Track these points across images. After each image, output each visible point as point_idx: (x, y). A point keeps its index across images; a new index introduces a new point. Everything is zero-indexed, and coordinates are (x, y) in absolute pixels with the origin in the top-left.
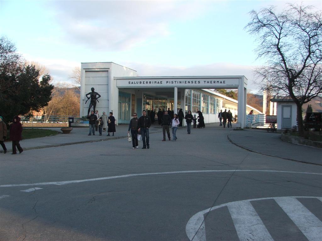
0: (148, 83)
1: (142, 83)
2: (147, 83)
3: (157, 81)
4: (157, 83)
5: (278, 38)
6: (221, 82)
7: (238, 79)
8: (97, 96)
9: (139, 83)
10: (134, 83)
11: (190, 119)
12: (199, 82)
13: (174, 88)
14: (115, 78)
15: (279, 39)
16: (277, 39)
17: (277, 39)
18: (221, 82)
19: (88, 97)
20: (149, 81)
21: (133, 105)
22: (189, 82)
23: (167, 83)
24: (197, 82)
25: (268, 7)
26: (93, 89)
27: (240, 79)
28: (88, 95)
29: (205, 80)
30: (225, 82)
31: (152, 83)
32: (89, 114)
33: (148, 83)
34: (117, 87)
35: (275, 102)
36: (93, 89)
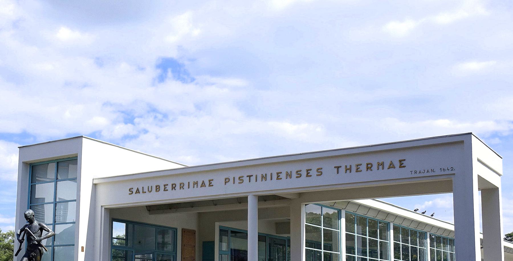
2: (383, 164)
4: (387, 165)
6: (392, 166)
10: (141, 190)
18: (203, 185)
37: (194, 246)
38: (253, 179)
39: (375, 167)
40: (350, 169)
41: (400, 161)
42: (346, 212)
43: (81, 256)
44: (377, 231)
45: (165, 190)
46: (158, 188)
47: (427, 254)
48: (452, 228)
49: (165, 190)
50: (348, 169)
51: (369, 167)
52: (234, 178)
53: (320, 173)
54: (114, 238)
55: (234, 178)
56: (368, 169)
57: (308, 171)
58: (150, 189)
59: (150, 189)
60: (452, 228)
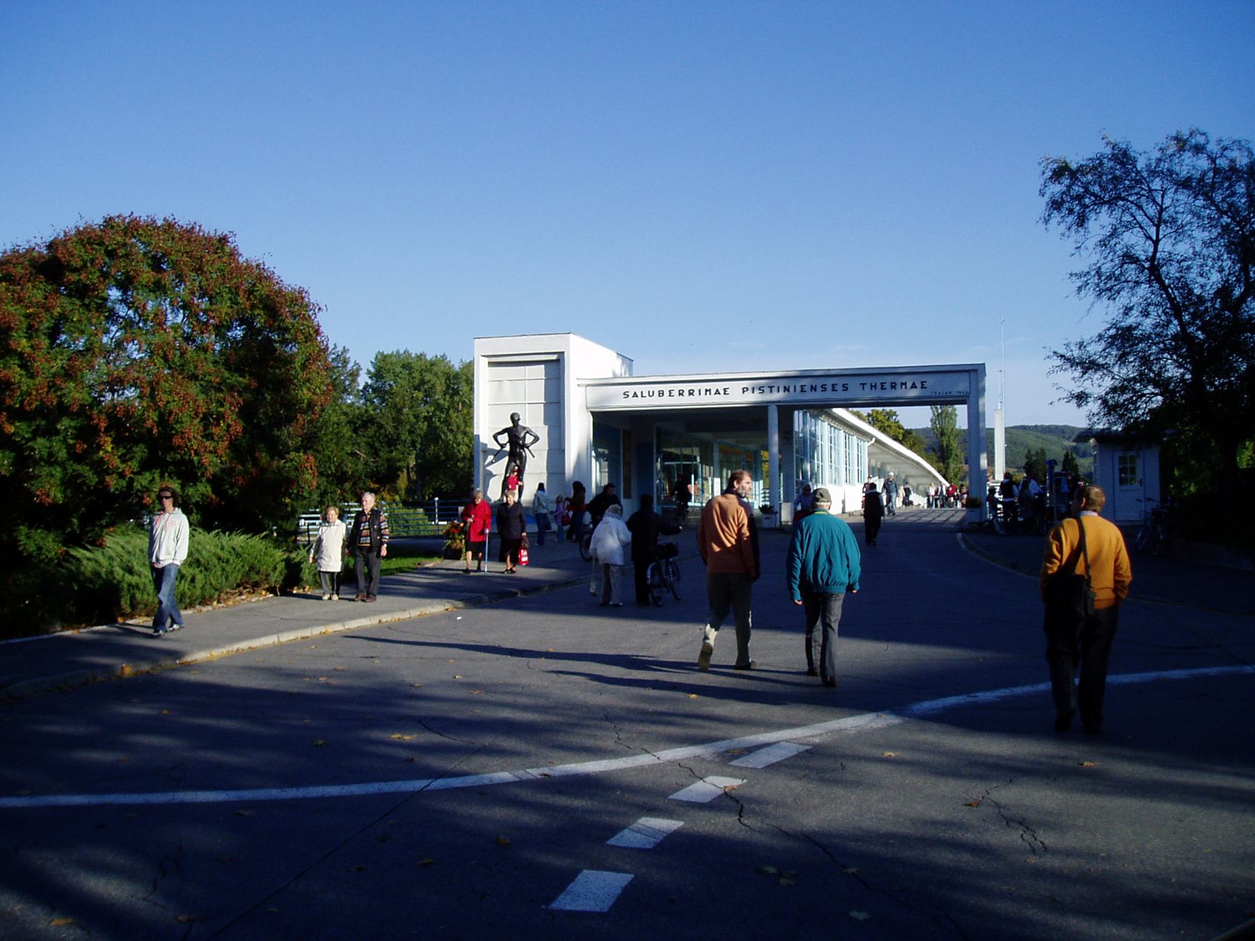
0: (686, 393)
1: (666, 393)
2: (690, 394)
3: (713, 386)
4: (713, 392)
5: (1154, 238)
6: (717, 392)
7: (966, 376)
8: (529, 439)
9: (656, 394)
10: (639, 395)
11: (1084, 500)
12: (845, 388)
13: (767, 407)
14: (580, 382)
15: (1156, 243)
16: (1151, 242)
17: (1149, 242)
18: (717, 392)
19: (501, 442)
20: (686, 387)
21: (627, 464)
22: (813, 388)
23: (744, 392)
24: (839, 388)
25: (1174, 134)
26: (514, 418)
27: (973, 375)
28: (499, 437)
29: (863, 380)
30: (926, 385)
31: (696, 393)
32: (522, 498)
33: (686, 393)
34: (587, 408)
35: (696, 446)
36: (514, 418)
37: (390, 628)
38: (775, 389)
39: (898, 387)
40: (875, 386)
41: (922, 382)
42: (773, 417)
43: (4, 642)
44: (684, 465)
45: (882, 389)
46: (824, 388)
47: (252, 650)
48: (761, 482)
49: (882, 389)
50: (873, 387)
51: (691, 393)
52: (700, 391)
53: (691, 393)
54: (743, 639)
55: (700, 391)
56: (680, 394)
57: (882, 384)
58: (651, 394)
59: (651, 394)
60: (761, 482)
